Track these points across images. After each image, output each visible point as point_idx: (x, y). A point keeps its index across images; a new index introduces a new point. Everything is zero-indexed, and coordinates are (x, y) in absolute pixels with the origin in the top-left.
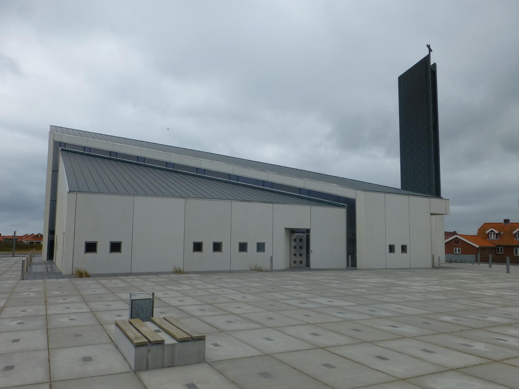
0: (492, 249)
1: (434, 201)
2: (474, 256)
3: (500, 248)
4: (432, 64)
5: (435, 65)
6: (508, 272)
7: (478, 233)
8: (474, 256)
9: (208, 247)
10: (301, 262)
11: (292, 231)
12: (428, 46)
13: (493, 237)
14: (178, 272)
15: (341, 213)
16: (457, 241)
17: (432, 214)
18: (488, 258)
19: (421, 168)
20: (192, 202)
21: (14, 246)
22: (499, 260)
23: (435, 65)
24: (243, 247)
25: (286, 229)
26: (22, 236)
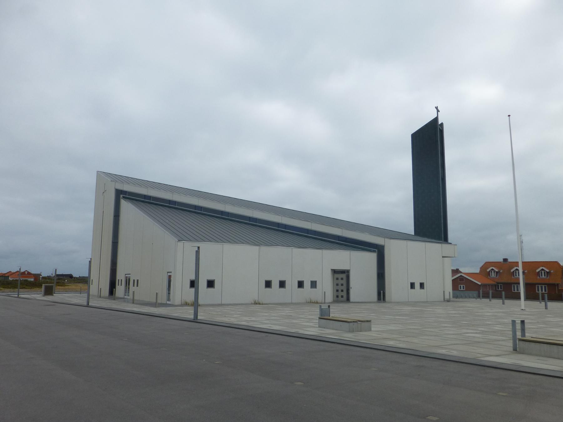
0: (492, 285)
1: (445, 246)
2: (477, 292)
3: (540, 286)
4: (440, 123)
5: (442, 124)
6: (503, 303)
7: (481, 271)
8: (477, 292)
9: (275, 284)
10: (342, 297)
11: (335, 272)
12: (437, 108)
13: (493, 275)
14: (256, 303)
15: (372, 257)
16: (461, 279)
17: (443, 257)
18: (488, 294)
19: (431, 216)
20: (264, 249)
21: (19, 284)
22: (497, 296)
23: (442, 124)
24: (301, 284)
25: (332, 270)
26: (14, 273)
